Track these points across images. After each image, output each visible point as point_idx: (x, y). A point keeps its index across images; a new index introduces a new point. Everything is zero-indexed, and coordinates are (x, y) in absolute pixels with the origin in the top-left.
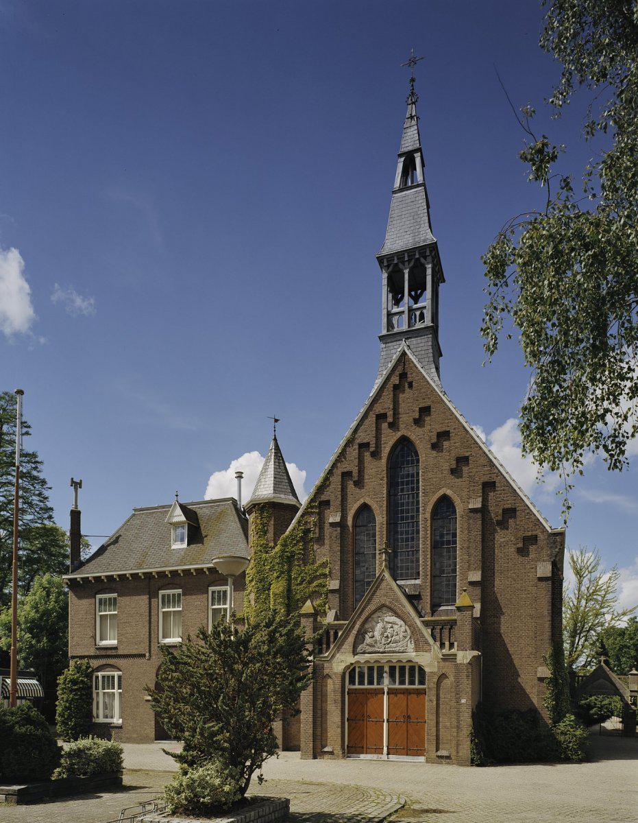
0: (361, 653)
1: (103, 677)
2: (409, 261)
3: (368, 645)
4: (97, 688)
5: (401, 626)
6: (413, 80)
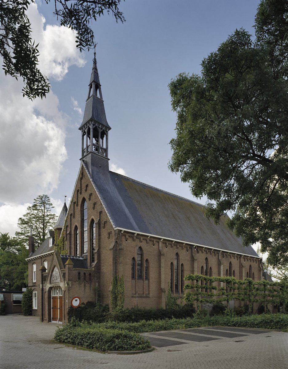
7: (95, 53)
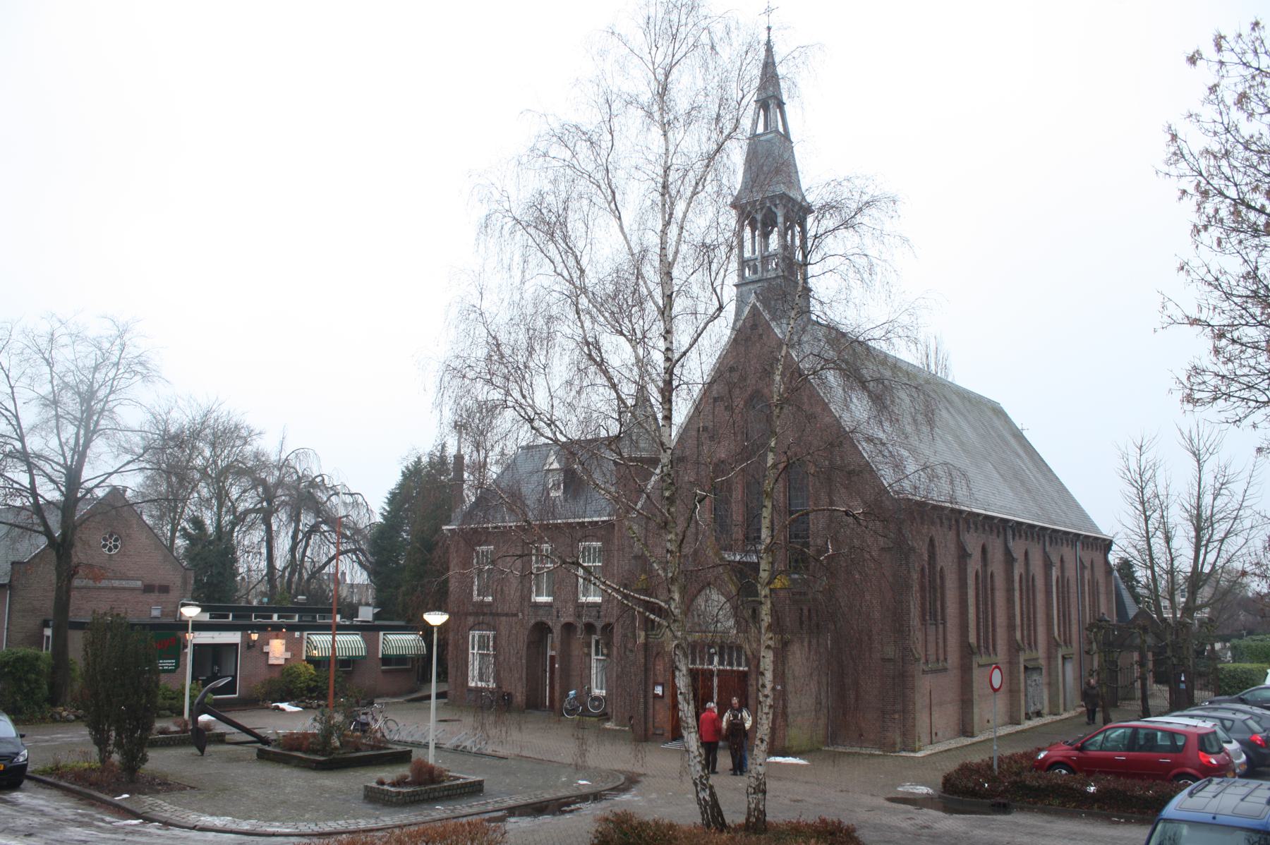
1: (480, 637)
2: (762, 209)
4: (473, 649)
6: (769, 29)
7: (769, 29)
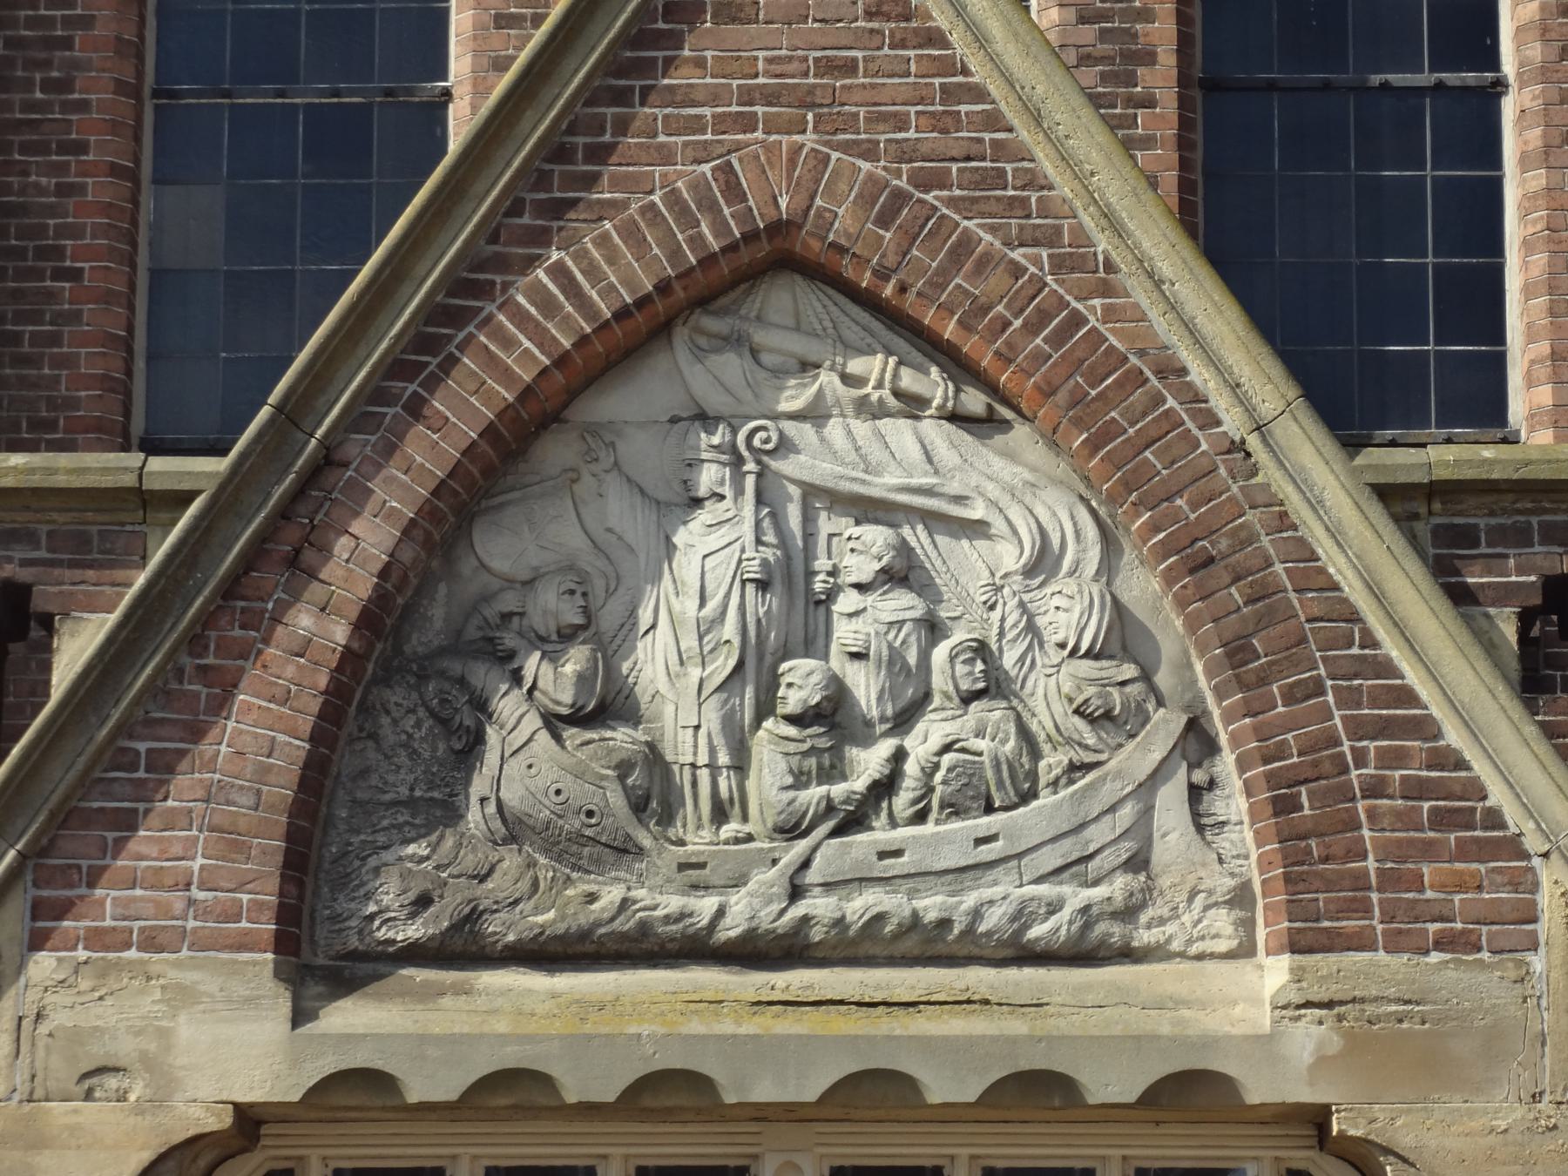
0: (415, 954)
3: (513, 829)
5: (1042, 564)
